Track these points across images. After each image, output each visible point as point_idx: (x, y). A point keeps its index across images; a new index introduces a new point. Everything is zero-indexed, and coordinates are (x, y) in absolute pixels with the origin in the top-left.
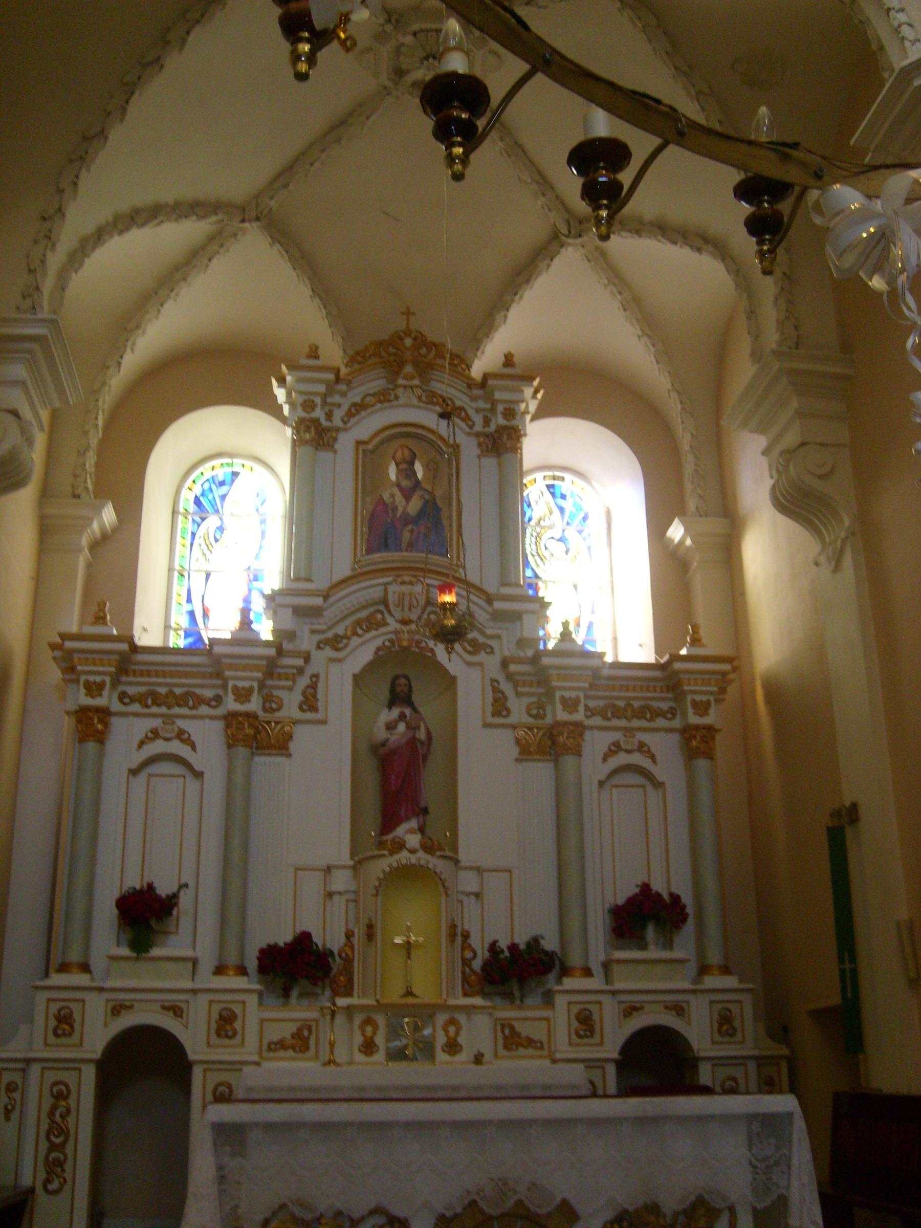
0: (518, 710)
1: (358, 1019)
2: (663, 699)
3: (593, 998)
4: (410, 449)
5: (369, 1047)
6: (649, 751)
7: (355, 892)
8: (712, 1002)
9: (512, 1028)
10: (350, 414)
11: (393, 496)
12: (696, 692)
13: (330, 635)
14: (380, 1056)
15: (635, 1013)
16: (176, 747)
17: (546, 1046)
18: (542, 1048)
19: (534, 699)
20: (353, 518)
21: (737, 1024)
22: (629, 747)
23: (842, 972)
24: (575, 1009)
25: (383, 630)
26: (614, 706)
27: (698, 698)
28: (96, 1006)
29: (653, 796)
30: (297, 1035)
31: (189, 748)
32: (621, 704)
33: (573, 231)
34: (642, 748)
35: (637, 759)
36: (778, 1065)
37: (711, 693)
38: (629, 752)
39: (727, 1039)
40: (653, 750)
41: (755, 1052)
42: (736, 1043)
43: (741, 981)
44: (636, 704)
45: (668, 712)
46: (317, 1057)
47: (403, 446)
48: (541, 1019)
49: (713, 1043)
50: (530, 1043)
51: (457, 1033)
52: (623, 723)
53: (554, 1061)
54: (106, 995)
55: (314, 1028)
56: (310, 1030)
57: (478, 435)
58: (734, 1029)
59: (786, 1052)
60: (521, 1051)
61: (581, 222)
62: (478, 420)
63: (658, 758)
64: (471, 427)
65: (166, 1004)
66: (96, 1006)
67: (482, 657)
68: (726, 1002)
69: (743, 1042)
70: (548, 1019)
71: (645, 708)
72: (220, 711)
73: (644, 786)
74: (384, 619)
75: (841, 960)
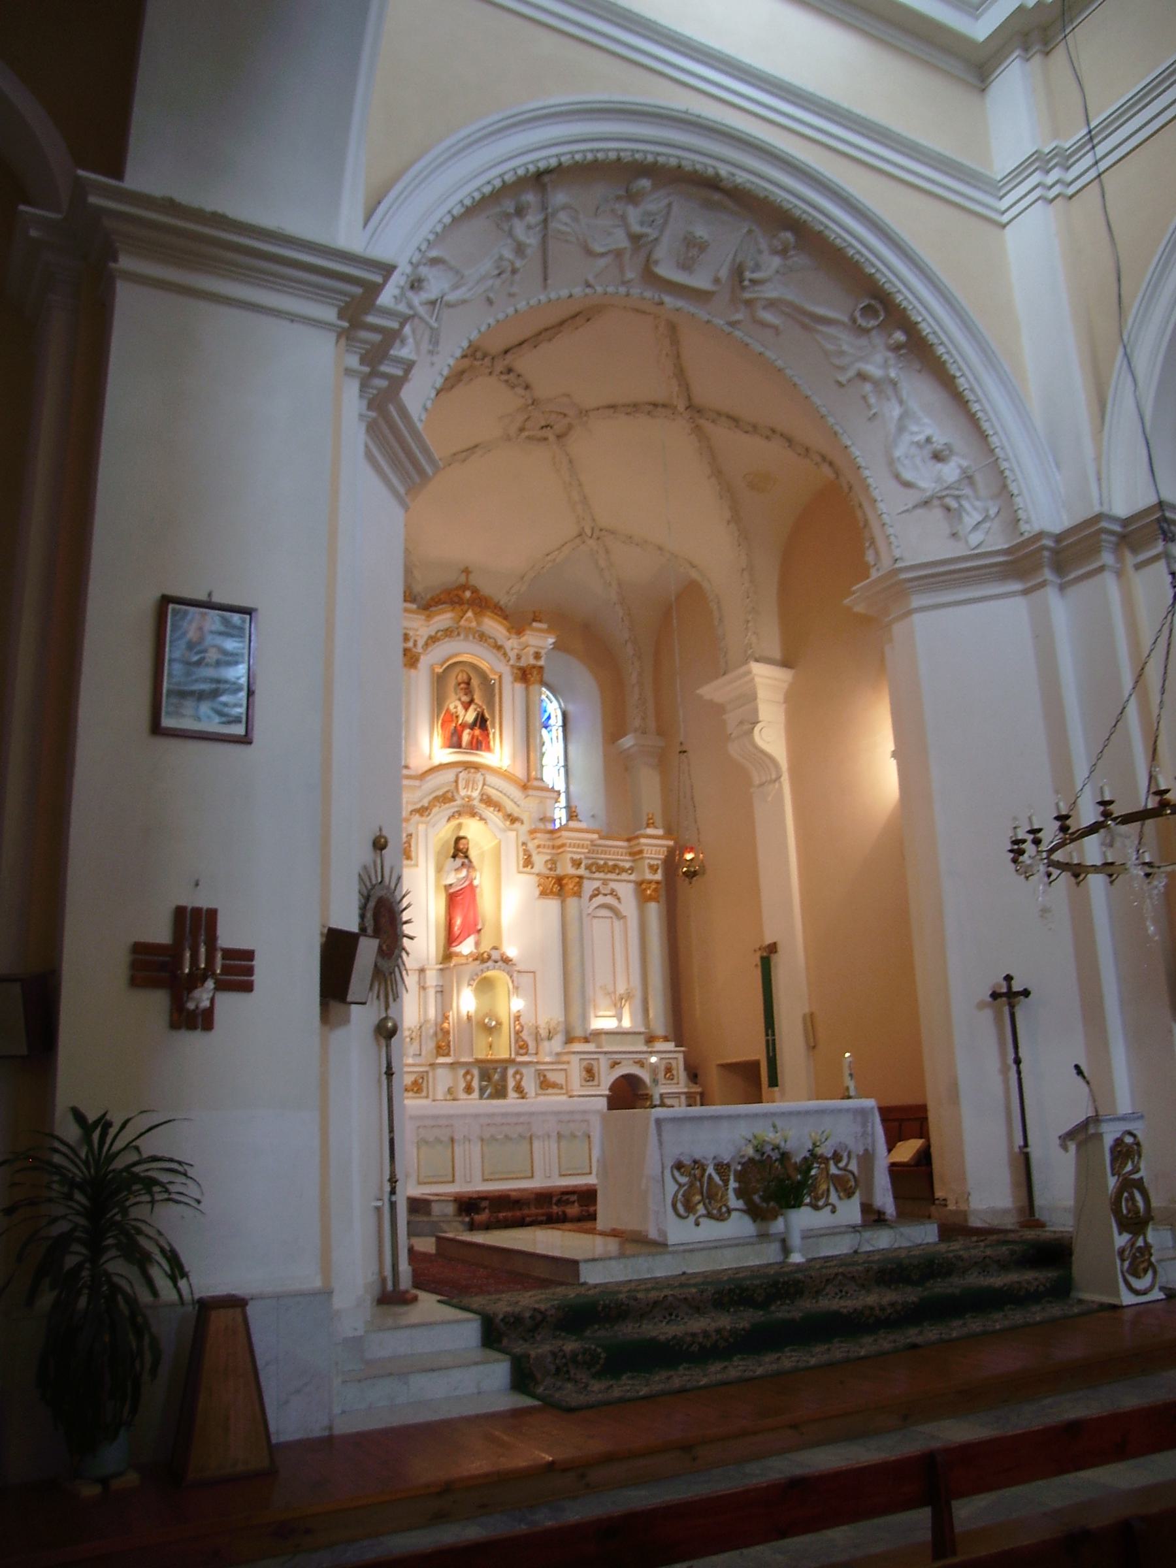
0: (539, 861)
1: (462, 1072)
2: (627, 861)
3: (595, 1056)
4: (467, 674)
5: (469, 1089)
6: (616, 895)
7: (442, 986)
8: (581, 1059)
9: (545, 1076)
10: (426, 645)
11: (456, 707)
12: (652, 858)
13: (418, 806)
14: (476, 1094)
15: (616, 1066)
16: (609, 900)
17: (564, 1087)
18: (562, 1088)
19: (548, 857)
20: (525, 731)
21: (675, 1072)
22: (606, 892)
23: (767, 1041)
24: (585, 1063)
25: (453, 804)
26: (597, 864)
27: (652, 862)
28: (603, 1064)
29: (618, 924)
30: (415, 1083)
31: (617, 901)
32: (602, 862)
33: (594, 536)
34: (613, 893)
35: (609, 900)
36: (695, 1098)
37: (584, 853)
38: (605, 895)
39: (669, 1082)
40: (620, 895)
41: (685, 1090)
42: (674, 1084)
43: (676, 1046)
44: (611, 863)
45: (629, 869)
46: (427, 1097)
47: (462, 671)
48: (561, 1070)
49: (582, 1086)
50: (554, 1085)
51: (521, 1079)
52: (601, 875)
53: (570, 1097)
54: (609, 1056)
55: (425, 1078)
56: (423, 1078)
57: (512, 666)
58: (673, 1075)
59: (699, 1090)
60: (550, 1091)
61: (601, 530)
62: (512, 655)
63: (622, 900)
64: (508, 661)
65: (636, 1060)
66: (603, 1064)
67: (517, 825)
68: (669, 1058)
69: (678, 1084)
70: (565, 1070)
71: (615, 866)
72: (633, 877)
73: (611, 917)
74: (453, 796)
75: (767, 1035)
